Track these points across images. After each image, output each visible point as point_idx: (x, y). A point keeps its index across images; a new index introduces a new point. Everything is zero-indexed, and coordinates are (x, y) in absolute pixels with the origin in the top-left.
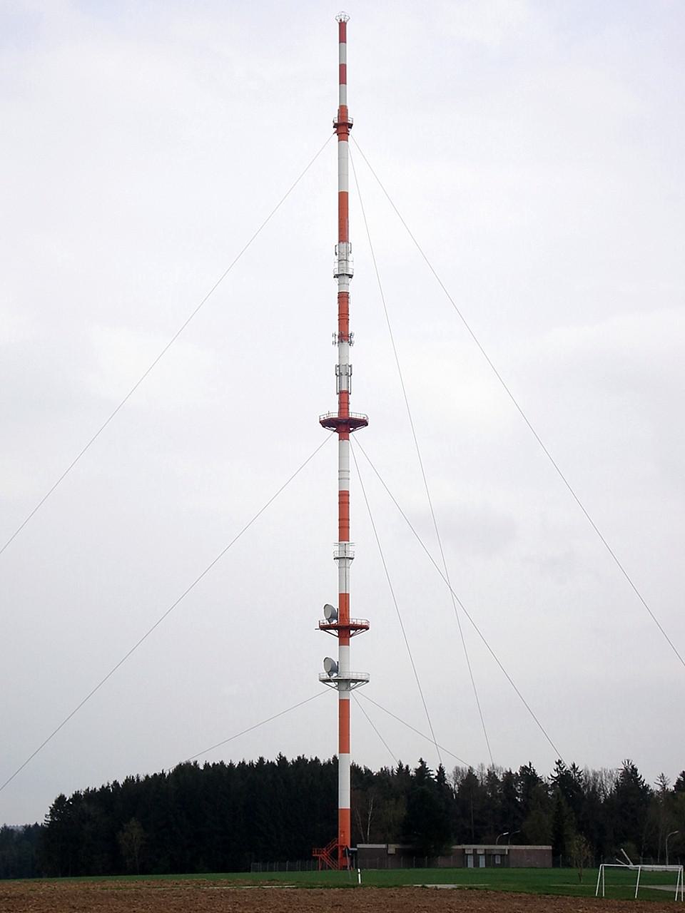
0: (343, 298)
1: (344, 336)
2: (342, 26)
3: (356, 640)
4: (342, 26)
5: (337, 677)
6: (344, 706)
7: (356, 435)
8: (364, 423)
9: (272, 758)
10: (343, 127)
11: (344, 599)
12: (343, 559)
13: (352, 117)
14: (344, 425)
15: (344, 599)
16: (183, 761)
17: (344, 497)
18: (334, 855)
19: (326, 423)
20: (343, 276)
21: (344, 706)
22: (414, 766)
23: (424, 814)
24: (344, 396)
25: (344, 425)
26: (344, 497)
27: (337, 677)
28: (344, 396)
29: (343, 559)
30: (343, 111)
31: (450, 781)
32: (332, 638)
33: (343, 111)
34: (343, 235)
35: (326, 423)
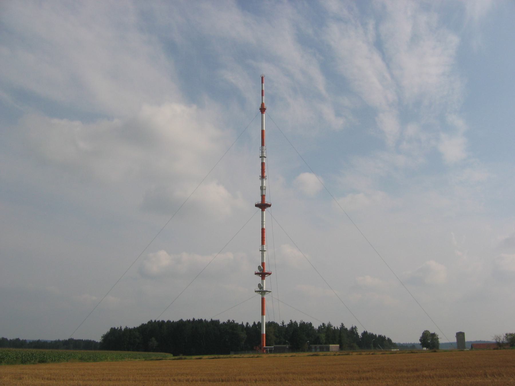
0: (263, 164)
1: (263, 177)
2: (262, 78)
3: (267, 278)
4: (262, 78)
5: (262, 292)
6: (263, 299)
7: (267, 210)
8: (269, 206)
9: (146, 322)
10: (263, 110)
11: (263, 264)
12: (263, 251)
13: (266, 106)
14: (263, 206)
15: (263, 264)
16: (5, 337)
17: (263, 230)
18: (260, 348)
19: (257, 206)
20: (262, 157)
21: (263, 299)
22: (191, 320)
23: (296, 338)
24: (263, 196)
25: (263, 206)
26: (263, 230)
27: (262, 292)
28: (263, 196)
29: (263, 251)
30: (262, 104)
31: (377, 336)
32: (259, 278)
33: (262, 104)
34: (263, 144)
35: (257, 206)
